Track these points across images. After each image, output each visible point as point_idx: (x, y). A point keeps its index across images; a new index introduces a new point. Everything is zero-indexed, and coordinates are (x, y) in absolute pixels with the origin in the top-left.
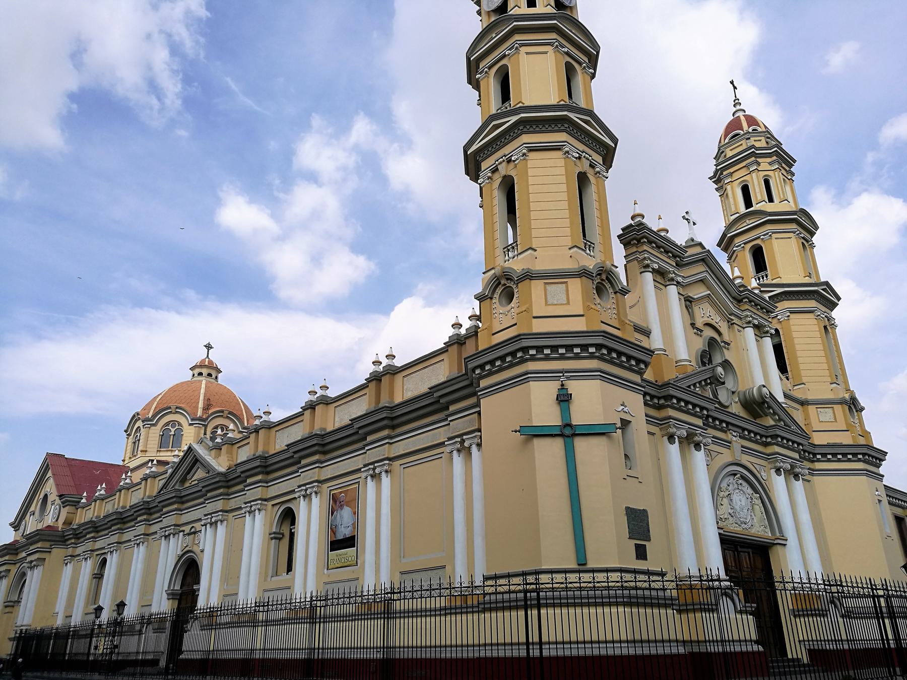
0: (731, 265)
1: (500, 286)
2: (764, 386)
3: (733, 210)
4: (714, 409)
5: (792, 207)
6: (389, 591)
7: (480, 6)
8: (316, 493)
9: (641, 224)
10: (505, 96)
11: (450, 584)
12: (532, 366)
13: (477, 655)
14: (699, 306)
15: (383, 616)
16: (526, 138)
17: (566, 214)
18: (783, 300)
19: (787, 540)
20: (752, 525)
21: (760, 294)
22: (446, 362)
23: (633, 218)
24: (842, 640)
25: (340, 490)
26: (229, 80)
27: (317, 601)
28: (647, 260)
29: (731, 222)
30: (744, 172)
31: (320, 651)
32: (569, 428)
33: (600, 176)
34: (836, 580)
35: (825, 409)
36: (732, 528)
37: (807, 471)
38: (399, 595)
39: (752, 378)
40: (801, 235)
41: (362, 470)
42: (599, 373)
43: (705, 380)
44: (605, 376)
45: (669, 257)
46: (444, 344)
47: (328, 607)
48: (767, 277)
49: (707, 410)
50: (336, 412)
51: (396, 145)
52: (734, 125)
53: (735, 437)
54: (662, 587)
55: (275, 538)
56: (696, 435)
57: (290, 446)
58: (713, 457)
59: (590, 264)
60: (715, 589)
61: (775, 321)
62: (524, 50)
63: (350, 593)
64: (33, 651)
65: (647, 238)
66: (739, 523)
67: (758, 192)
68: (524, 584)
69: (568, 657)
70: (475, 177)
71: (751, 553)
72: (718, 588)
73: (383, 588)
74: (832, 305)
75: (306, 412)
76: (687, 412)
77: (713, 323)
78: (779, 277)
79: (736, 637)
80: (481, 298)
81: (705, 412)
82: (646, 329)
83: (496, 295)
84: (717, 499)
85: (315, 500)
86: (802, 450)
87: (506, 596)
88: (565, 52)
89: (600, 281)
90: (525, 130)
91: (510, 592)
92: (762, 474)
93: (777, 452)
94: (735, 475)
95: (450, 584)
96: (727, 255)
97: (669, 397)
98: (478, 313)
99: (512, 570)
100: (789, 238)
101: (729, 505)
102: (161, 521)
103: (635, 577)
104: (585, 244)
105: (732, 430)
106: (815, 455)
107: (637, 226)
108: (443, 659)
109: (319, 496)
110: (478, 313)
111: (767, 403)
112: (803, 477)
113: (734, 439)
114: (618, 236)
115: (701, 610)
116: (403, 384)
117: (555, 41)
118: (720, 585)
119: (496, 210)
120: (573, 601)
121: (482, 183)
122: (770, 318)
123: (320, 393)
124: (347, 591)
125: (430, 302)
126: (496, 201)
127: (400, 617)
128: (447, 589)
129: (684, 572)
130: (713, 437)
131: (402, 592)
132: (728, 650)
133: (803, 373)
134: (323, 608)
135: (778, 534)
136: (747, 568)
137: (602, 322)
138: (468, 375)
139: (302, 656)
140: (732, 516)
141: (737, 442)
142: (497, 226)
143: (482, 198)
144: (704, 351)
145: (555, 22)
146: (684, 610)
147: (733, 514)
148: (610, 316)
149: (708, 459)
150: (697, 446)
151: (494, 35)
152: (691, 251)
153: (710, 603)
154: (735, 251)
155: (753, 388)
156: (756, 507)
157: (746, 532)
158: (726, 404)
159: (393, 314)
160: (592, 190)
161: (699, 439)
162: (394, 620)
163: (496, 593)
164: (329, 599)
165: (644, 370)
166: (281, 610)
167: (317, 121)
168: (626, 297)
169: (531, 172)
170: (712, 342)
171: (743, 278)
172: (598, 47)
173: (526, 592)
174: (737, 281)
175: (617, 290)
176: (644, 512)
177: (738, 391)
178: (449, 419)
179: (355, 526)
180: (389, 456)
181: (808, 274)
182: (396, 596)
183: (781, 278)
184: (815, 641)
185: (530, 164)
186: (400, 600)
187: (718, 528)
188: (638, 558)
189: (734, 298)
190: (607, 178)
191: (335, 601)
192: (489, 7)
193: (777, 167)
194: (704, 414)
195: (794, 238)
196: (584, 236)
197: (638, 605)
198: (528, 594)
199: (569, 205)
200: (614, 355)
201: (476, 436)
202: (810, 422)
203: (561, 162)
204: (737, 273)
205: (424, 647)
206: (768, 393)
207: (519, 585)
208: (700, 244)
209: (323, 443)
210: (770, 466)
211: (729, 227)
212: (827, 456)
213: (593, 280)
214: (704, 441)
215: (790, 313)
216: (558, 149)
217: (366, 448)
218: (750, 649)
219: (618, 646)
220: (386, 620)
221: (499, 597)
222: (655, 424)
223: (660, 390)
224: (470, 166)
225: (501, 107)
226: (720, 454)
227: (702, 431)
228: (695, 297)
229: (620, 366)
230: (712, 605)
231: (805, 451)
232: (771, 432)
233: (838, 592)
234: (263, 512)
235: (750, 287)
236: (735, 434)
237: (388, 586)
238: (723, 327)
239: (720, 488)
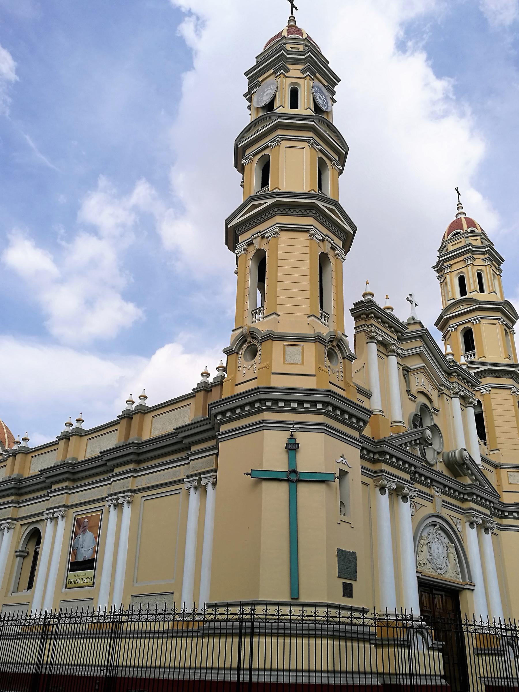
0: (445, 343)
1: (246, 343)
2: (465, 450)
3: (450, 296)
4: (421, 466)
5: (499, 298)
6: (118, 613)
7: (251, 102)
8: (63, 517)
9: (371, 301)
10: (265, 181)
11: (174, 610)
12: (267, 416)
13: (192, 677)
14: (414, 376)
15: (110, 635)
16: (279, 219)
17: (308, 287)
18: (486, 377)
19: (475, 586)
20: (446, 571)
21: (467, 370)
22: (193, 406)
23: (364, 296)
24: (513, 678)
25: (84, 516)
26: (27, 137)
27: (50, 618)
28: (373, 333)
29: (447, 306)
30: (461, 265)
31: (48, 666)
32: (294, 474)
33: (339, 257)
34: (511, 625)
35: (514, 473)
36: (429, 573)
37: (495, 526)
38: (127, 617)
39: (456, 441)
40: (504, 323)
41: (107, 499)
42: (324, 427)
43: (415, 441)
44: (329, 431)
45: (392, 332)
46: (193, 390)
47: (60, 625)
48: (474, 356)
49: (415, 467)
50: (89, 444)
51: (171, 210)
52: (456, 225)
53: (438, 492)
55: (20, 556)
56: (404, 488)
57: (42, 472)
58: (417, 509)
59: (324, 331)
60: (408, 628)
61: (478, 394)
62: (284, 143)
63: (82, 613)
65: (374, 314)
66: (435, 568)
67: (471, 283)
68: (240, 614)
69: (369, 686)
70: (233, 248)
71: (444, 596)
72: (410, 628)
73: (113, 610)
75: (60, 442)
76: (398, 468)
78: (484, 357)
79: (423, 672)
80: (228, 352)
81: (413, 469)
82: (368, 392)
83: (242, 351)
84: (418, 546)
85: (61, 523)
86: (493, 507)
87: (224, 624)
88: (318, 149)
89: (331, 347)
90: (279, 212)
91: (227, 620)
92: (458, 526)
93: (472, 508)
94: (435, 525)
95: (174, 610)
96: (443, 334)
97: (383, 453)
98: (225, 365)
99: (230, 600)
100: (495, 324)
101: (428, 552)
102: (111, 483)
103: (351, 614)
104: (322, 314)
105: (435, 486)
106: (503, 512)
107: (366, 303)
108: (181, 681)
109: (64, 519)
110: (225, 365)
111: (466, 464)
112: (492, 531)
113: (437, 494)
114: (350, 310)
115: (394, 645)
116: (151, 424)
117: (311, 139)
118: (413, 624)
119: (249, 277)
120: (264, 631)
121: (238, 254)
122: (474, 391)
123: (75, 425)
124: (79, 611)
125: (188, 349)
126: (249, 270)
127: (126, 638)
128: (171, 614)
129: (381, 610)
130: (418, 491)
131: (130, 615)
132: (415, 683)
133: (498, 440)
134: (55, 626)
135: (468, 580)
136: (440, 609)
137: (330, 382)
138: (210, 420)
139: (32, 670)
140: (430, 562)
141: (439, 497)
142: (248, 291)
143: (237, 266)
144: (416, 415)
145: (313, 123)
146: (386, 644)
147: (430, 560)
148: (338, 378)
149: (413, 510)
150: (405, 498)
151: (260, 128)
152: (411, 328)
153: (402, 639)
154: (449, 331)
155: (455, 451)
156: (451, 555)
157: (440, 577)
158: (432, 463)
159: (154, 358)
160: (331, 269)
161: (406, 492)
162: (120, 640)
163: (215, 620)
164: (62, 618)
165: (363, 428)
166: (15, 626)
167: (103, 181)
168: (352, 363)
169: (280, 249)
170: (424, 408)
171: (454, 355)
172: (347, 148)
173: (241, 621)
174: (449, 357)
175: (345, 356)
176: (354, 553)
177: (443, 452)
178: (50, 495)
179: (96, 550)
180: (131, 488)
181: (508, 357)
182: (124, 618)
183: (486, 357)
184: (490, 678)
185: (281, 241)
186: (128, 622)
187: (417, 572)
188: (345, 595)
189: (445, 371)
190: (345, 260)
191: (68, 620)
192: (258, 104)
193: (489, 263)
194: (413, 470)
195: (498, 324)
196: (321, 307)
197: (340, 638)
198: (244, 624)
199: (310, 280)
200: (338, 412)
201: (212, 476)
202: (501, 484)
203: (307, 243)
204: (449, 350)
205: (182, 668)
206: (468, 456)
207: (236, 614)
208: (420, 323)
209: (73, 471)
210: (465, 520)
211: (446, 310)
212: (512, 514)
213: (325, 345)
214: (410, 494)
215: (491, 388)
216: (305, 231)
217: (112, 479)
218: (439, 683)
219: (357, 676)
220: (112, 640)
221: (218, 624)
223: (376, 446)
224: (229, 237)
225: (261, 190)
226: (423, 507)
227: (410, 485)
228: (412, 368)
229: (343, 422)
230: (404, 641)
231: (495, 508)
232: (468, 490)
233: (512, 636)
234: (12, 531)
235: (459, 362)
236: (437, 489)
237: (118, 608)
238: (434, 395)
239: (421, 536)
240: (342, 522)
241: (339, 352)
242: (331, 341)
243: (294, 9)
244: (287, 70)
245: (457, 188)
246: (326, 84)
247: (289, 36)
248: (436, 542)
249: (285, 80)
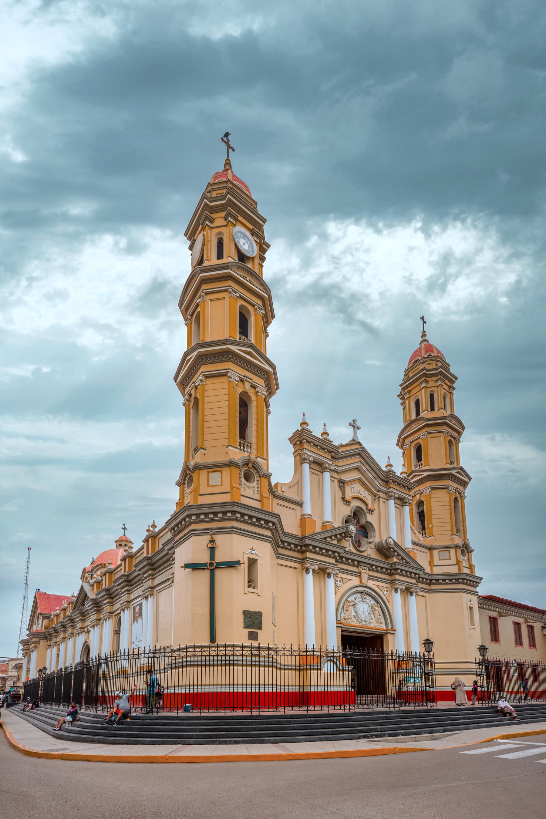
12: (193, 527)
14: (351, 486)
19: (395, 631)
40: (448, 434)
54: (241, 654)
56: (327, 568)
58: (344, 582)
64: (84, 695)
65: (306, 439)
67: (424, 404)
74: (464, 484)
77: (362, 497)
88: (238, 297)
113: (363, 571)
147: (356, 616)
183: (429, 465)
185: (207, 387)
189: (382, 480)
208: (359, 443)
222: (297, 562)
228: (347, 480)
234: (111, 620)
238: (369, 499)
240: (249, 593)
241: (256, 472)
242: (247, 464)
243: (230, 150)
244: (212, 221)
245: (423, 316)
246: (251, 227)
247: (216, 181)
248: (361, 603)
249: (211, 232)
